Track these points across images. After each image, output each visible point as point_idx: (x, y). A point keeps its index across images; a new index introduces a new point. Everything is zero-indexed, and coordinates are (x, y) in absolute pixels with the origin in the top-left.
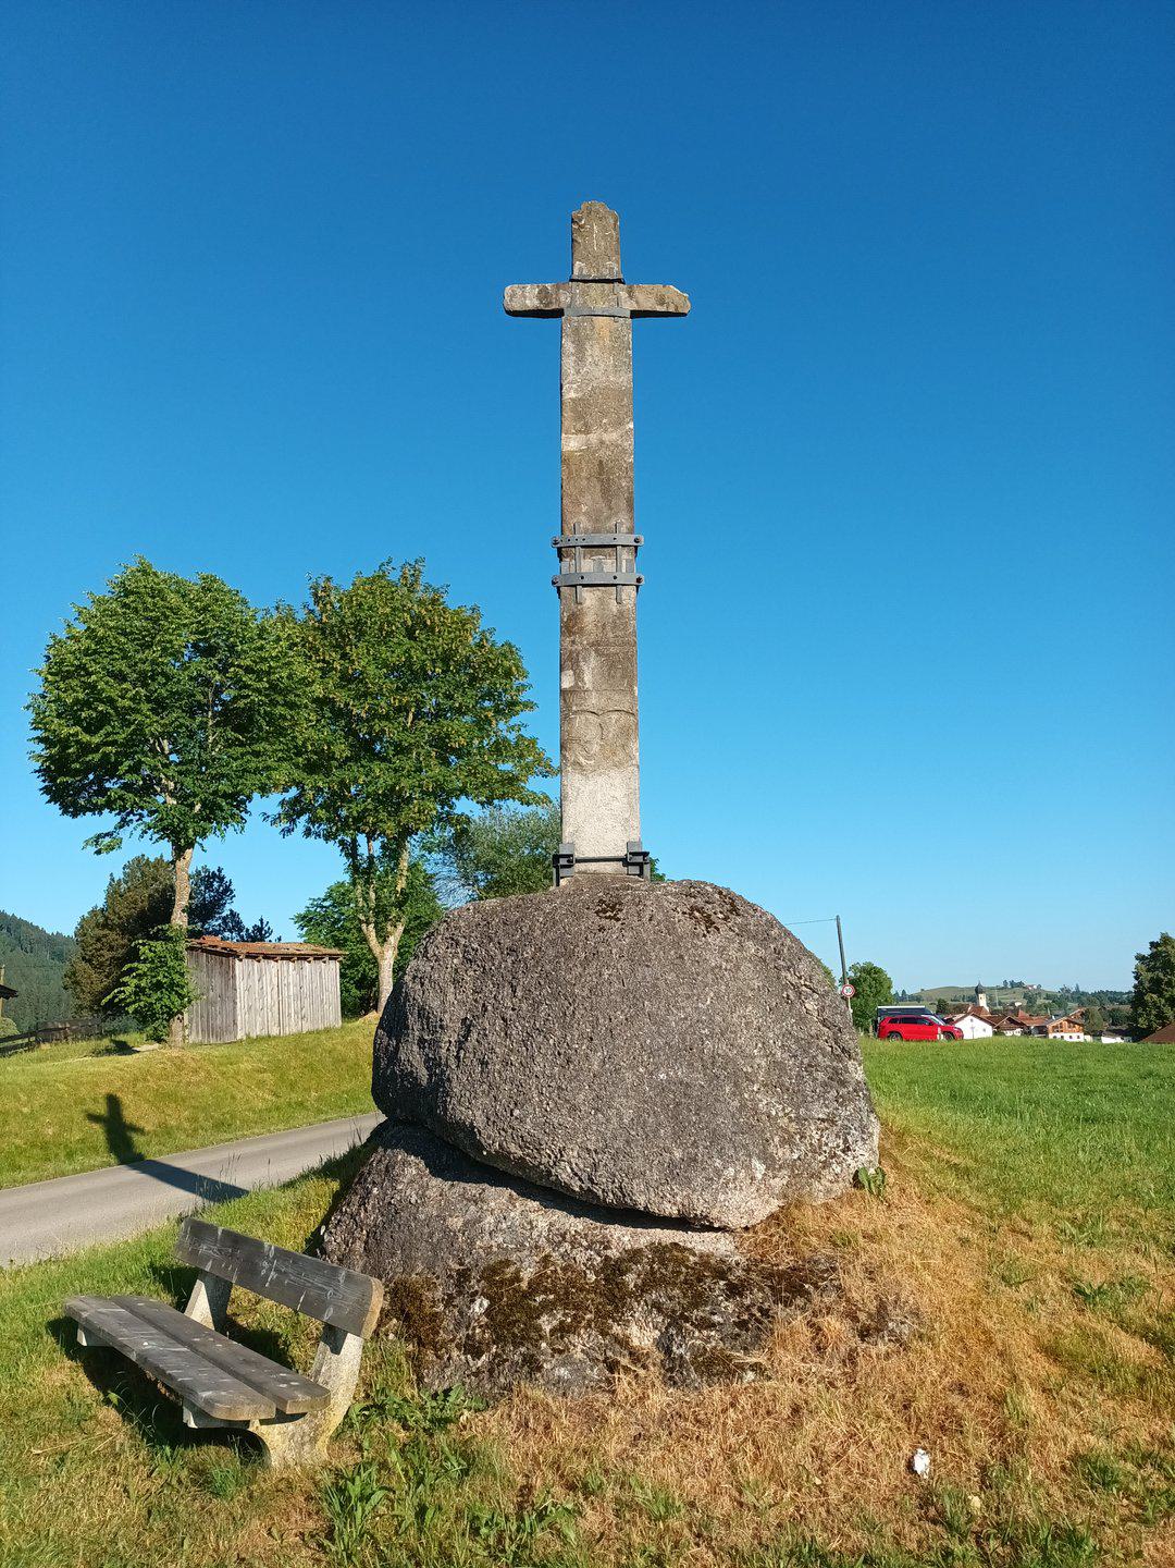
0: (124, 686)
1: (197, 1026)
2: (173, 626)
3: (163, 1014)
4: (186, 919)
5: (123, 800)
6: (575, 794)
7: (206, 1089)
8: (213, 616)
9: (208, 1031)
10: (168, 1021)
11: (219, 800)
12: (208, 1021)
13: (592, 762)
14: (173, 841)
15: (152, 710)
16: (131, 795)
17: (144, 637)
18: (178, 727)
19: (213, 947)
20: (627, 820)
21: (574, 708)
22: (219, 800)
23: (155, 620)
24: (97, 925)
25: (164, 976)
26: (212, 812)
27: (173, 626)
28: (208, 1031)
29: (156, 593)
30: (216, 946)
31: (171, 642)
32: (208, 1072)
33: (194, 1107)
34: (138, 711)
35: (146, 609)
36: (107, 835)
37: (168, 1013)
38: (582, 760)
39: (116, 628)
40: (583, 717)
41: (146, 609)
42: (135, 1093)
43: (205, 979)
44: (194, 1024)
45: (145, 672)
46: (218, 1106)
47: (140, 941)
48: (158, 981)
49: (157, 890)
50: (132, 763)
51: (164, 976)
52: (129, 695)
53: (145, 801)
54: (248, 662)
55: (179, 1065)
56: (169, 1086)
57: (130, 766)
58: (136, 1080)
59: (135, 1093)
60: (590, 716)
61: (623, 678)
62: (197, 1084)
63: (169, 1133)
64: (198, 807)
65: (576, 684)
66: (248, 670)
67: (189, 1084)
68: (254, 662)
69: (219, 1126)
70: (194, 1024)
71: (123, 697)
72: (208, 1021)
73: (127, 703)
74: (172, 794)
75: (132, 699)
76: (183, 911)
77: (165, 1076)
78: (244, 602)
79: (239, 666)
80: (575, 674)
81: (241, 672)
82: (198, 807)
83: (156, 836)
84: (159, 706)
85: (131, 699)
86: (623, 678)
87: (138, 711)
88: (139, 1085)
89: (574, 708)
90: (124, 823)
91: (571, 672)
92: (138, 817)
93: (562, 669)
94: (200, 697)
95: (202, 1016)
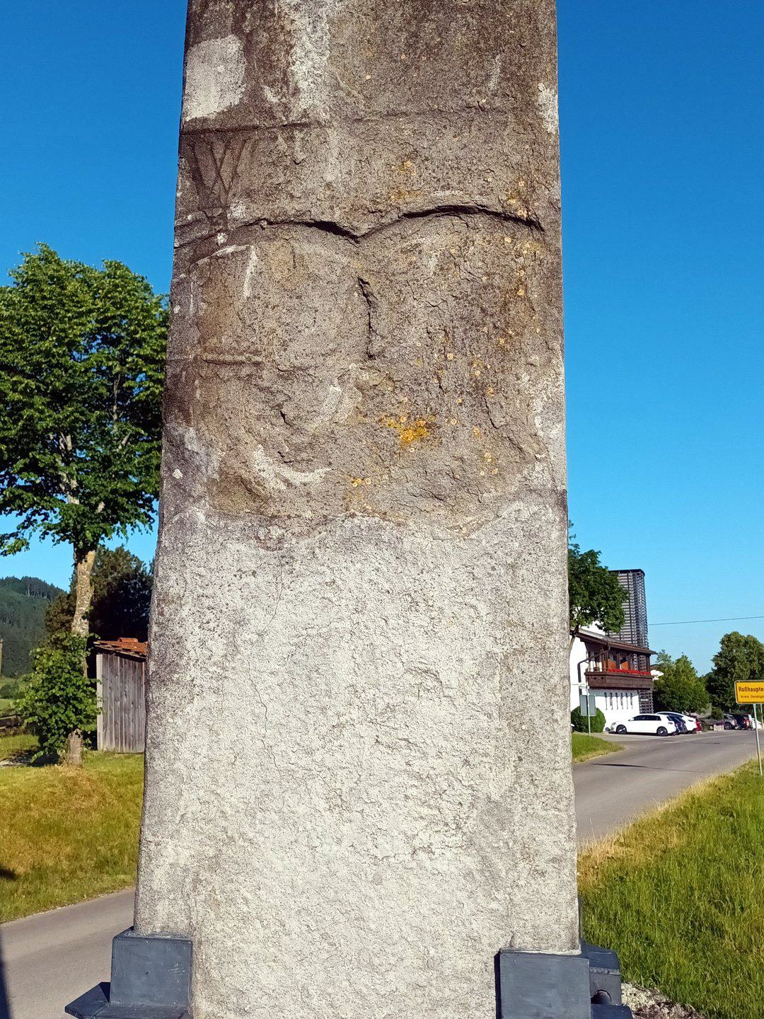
0: (15, 379)
1: (111, 733)
2: (70, 315)
3: (59, 729)
4: (86, 627)
5: (22, 499)
6: (218, 647)
7: (96, 816)
8: (114, 304)
9: (122, 738)
10: (66, 736)
11: (120, 499)
12: (121, 729)
13: (314, 477)
14: (74, 543)
15: (48, 405)
16: (30, 494)
17: (40, 327)
18: (73, 421)
19: (127, 650)
20: (497, 813)
21: (239, 211)
22: (120, 499)
23: (51, 309)
24: (63, 611)
25: (60, 689)
26: (114, 512)
27: (70, 315)
28: (122, 738)
29: (59, 282)
30: (129, 650)
31: (63, 330)
32: (103, 796)
33: (78, 841)
34: (31, 406)
35: (44, 298)
36: (12, 535)
37: (65, 728)
38: (262, 465)
39: (11, 318)
40: (278, 252)
41: (44, 298)
42: (12, 826)
43: (119, 684)
44: (108, 731)
45: (39, 364)
46: (107, 837)
47: (38, 650)
48: (54, 695)
49: (115, 579)
50: (27, 461)
51: (60, 689)
52: (20, 387)
53: (46, 501)
54: (148, 351)
55: (72, 787)
56: (53, 814)
57: (25, 464)
58: (17, 808)
59: (12, 826)
60: (317, 249)
61: (482, 48)
62: (87, 812)
63: (41, 878)
64: (101, 506)
65: (254, 95)
66: (147, 359)
67: (77, 811)
68: (154, 350)
69: (103, 865)
70: (108, 731)
71: (15, 391)
72: (121, 729)
73: (17, 396)
74: (75, 493)
75: (23, 392)
76: (84, 618)
77: (53, 802)
78: (147, 288)
79: (138, 356)
80: (247, 50)
81: (140, 362)
82: (101, 506)
83: (57, 537)
84: (58, 399)
85: (21, 393)
86: (482, 48)
87: (31, 406)
88: (20, 815)
89: (239, 211)
90: (29, 523)
91: (232, 45)
92: (43, 517)
93: (193, 34)
94: (103, 390)
95: (116, 723)
